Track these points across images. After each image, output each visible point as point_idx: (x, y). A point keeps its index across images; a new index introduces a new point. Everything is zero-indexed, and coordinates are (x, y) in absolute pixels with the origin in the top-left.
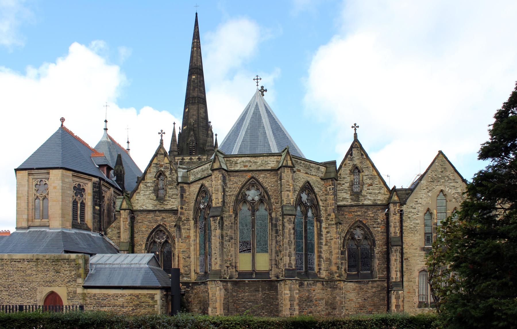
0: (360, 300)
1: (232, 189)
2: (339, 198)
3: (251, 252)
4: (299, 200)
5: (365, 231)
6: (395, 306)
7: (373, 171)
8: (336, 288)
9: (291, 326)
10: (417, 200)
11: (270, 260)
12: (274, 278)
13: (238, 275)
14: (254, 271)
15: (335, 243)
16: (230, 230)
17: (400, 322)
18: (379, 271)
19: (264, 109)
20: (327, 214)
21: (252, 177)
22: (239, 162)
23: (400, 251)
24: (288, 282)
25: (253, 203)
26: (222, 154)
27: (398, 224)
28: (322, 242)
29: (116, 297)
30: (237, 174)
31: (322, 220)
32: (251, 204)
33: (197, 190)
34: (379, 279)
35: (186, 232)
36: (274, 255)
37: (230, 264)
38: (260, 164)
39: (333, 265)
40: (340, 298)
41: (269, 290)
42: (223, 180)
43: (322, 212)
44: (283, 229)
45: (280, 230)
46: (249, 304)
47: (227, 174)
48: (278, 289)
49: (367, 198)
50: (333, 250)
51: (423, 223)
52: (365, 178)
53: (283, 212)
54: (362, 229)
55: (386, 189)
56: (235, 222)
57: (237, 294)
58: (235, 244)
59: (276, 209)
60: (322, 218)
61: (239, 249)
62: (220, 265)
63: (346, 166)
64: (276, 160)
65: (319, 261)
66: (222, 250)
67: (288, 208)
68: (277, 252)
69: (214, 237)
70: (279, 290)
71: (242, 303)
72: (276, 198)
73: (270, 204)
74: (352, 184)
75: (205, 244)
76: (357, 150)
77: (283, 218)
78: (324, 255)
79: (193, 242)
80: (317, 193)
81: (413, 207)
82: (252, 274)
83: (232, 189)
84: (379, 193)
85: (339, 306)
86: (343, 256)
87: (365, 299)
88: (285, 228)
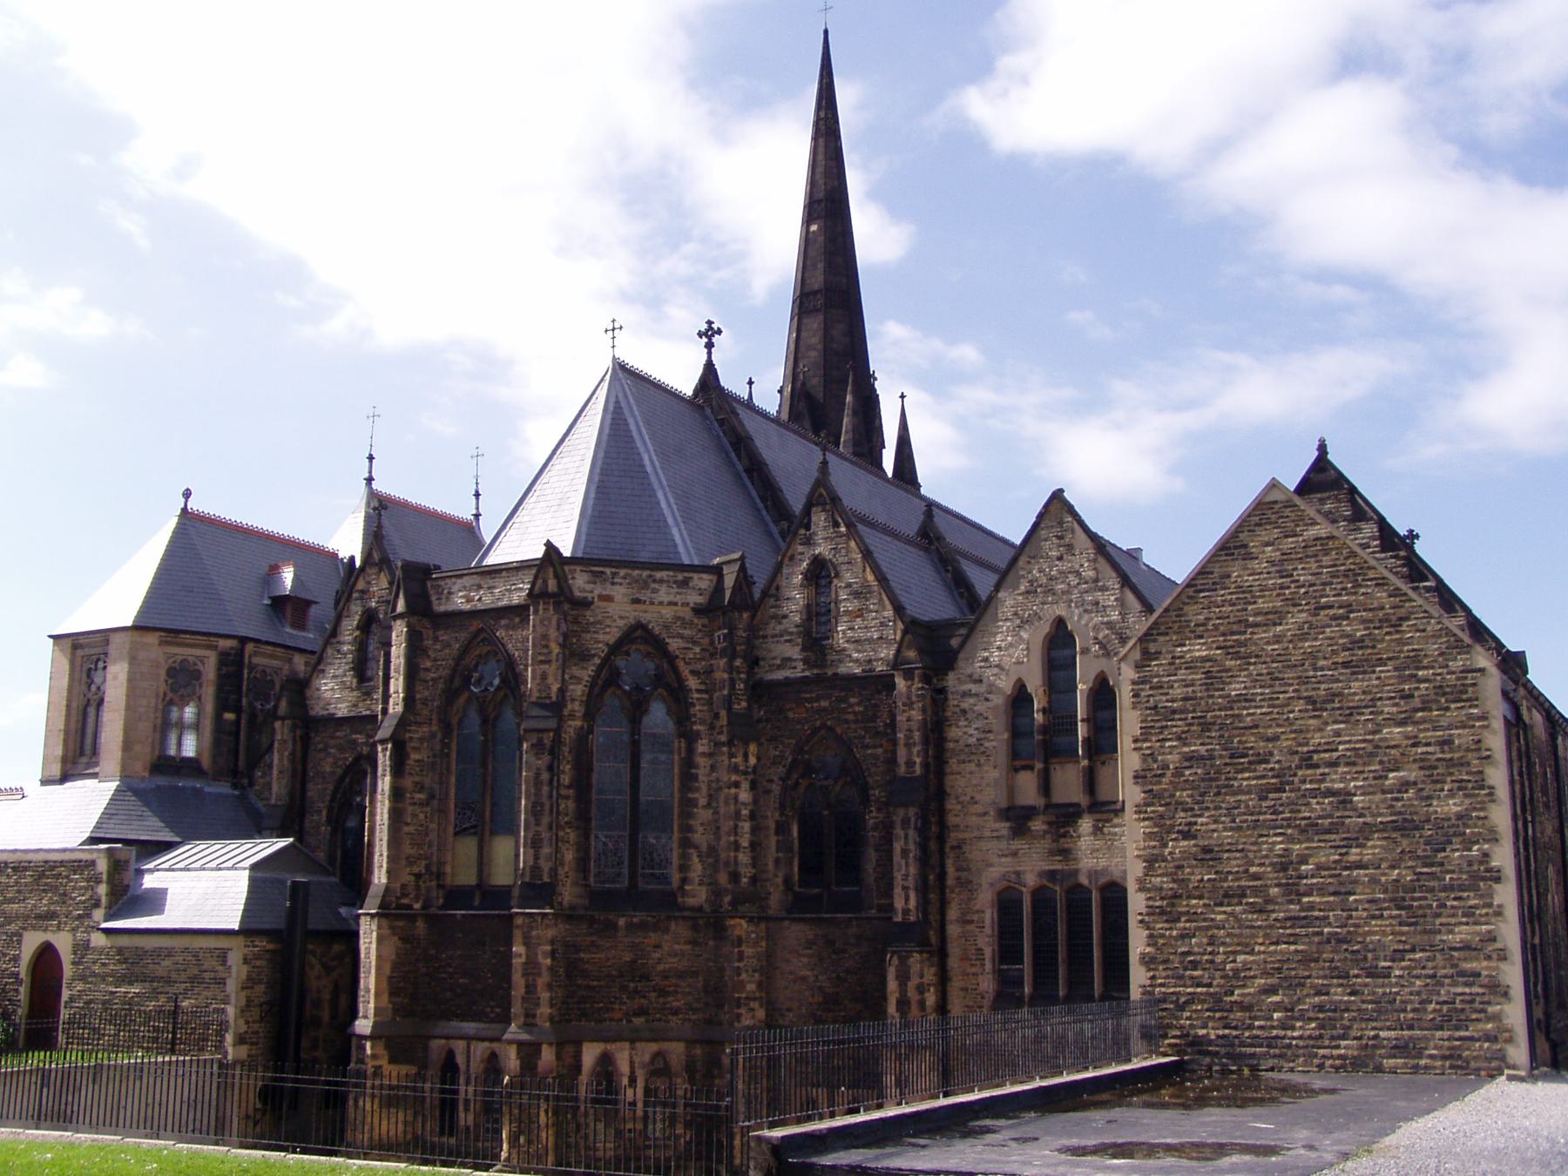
14: (479, 886)
28: (697, 799)
37: (427, 867)
43: (698, 708)
65: (684, 856)
78: (700, 837)
80: (677, 653)
81: (976, 676)
87: (838, 977)
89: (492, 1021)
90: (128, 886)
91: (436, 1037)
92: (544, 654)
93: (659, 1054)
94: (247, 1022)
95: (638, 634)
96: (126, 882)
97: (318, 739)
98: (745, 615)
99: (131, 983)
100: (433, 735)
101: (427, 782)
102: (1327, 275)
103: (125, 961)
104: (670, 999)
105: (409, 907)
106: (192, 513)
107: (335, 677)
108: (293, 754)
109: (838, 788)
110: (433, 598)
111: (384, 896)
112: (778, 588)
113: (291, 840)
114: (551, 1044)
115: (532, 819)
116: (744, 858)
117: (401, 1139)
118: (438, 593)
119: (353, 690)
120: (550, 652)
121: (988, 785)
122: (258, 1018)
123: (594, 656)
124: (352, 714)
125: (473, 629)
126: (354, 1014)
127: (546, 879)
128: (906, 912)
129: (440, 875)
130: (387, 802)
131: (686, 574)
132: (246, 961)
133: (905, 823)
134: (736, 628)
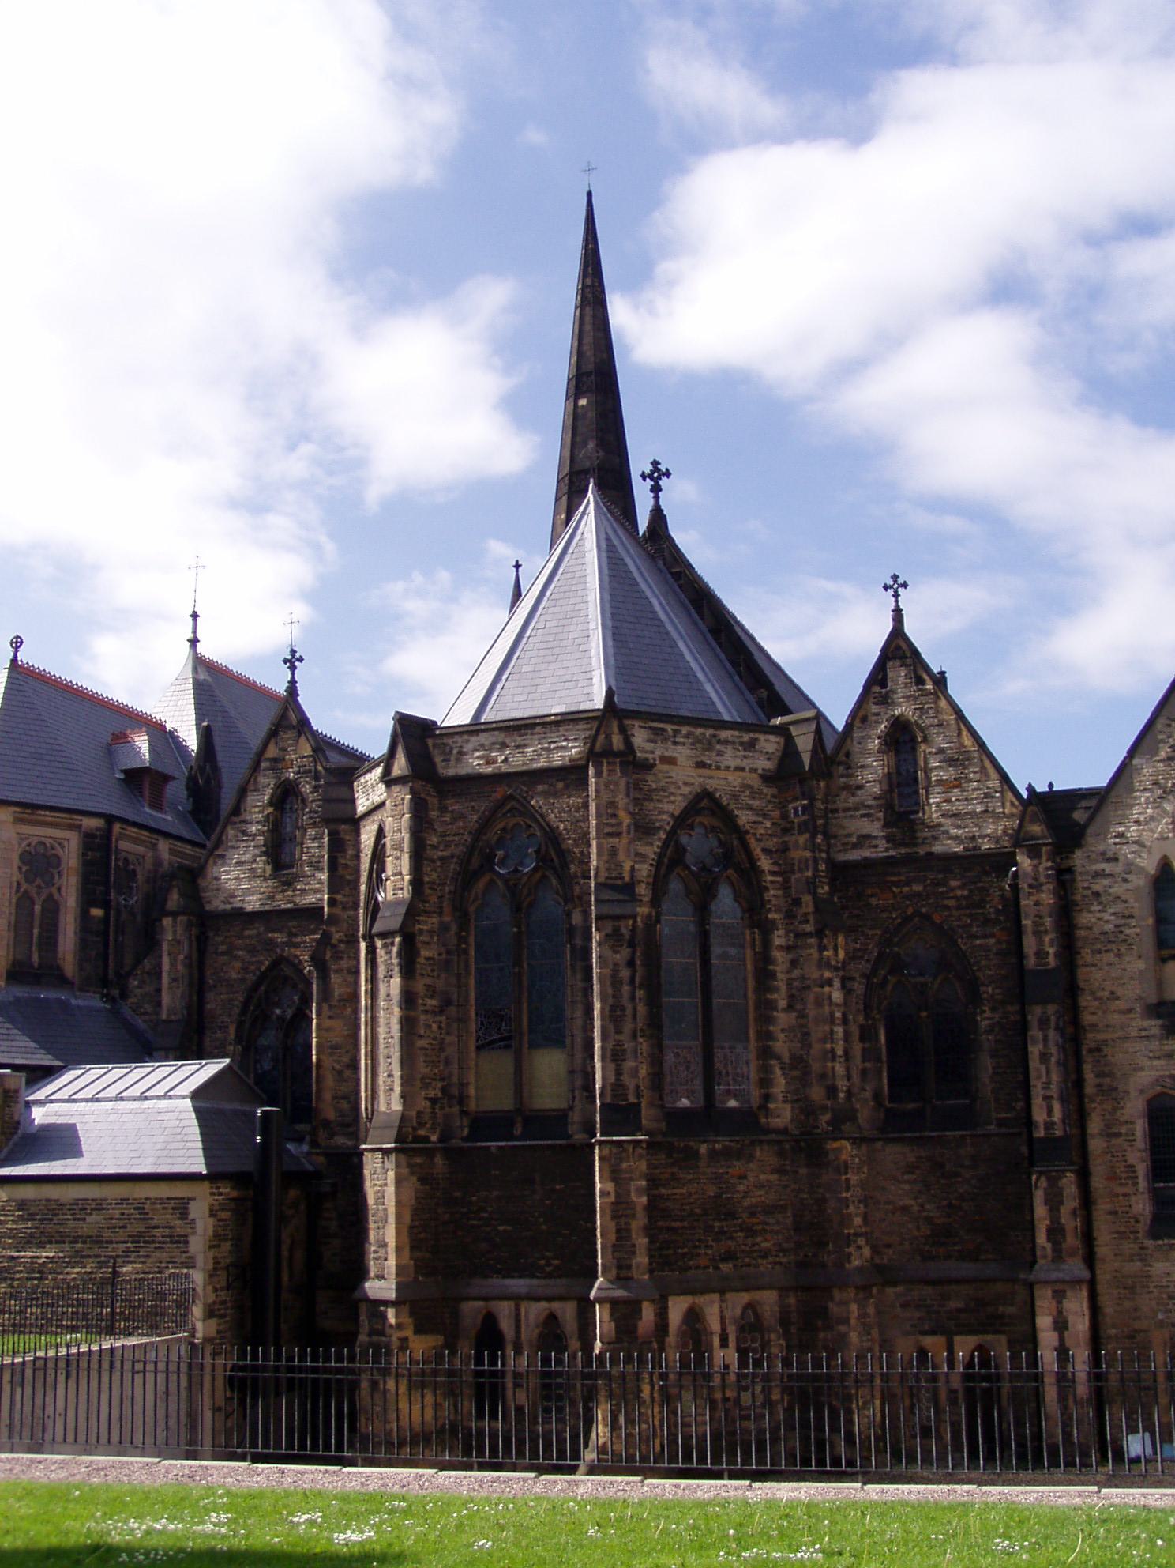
1: (451, 839)
13: (471, 1127)
28: (776, 1001)
29: (81, 1209)
37: (444, 1090)
46: (501, 1228)
65: (765, 1069)
80: (748, 827)
81: (1110, 854)
87: (950, 1206)
89: (549, 1276)
90: (18, 1123)
91: (468, 1299)
92: (613, 825)
93: (750, 1306)
94: (215, 1290)
95: (705, 804)
96: (16, 1118)
97: (219, 939)
98: (822, 784)
99: (41, 1245)
100: (444, 928)
101: (440, 985)
102: (942, 504)
103: (31, 1217)
104: (759, 1239)
105: (426, 1139)
106: (22, 667)
107: (240, 863)
108: (188, 957)
109: (936, 986)
110: (438, 760)
111: (400, 1127)
112: (848, 755)
113: (228, 1061)
114: (653, 1301)
115: (611, 1027)
116: (840, 1069)
117: (417, 1427)
118: (444, 753)
119: (266, 879)
120: (620, 824)
121: (1131, 978)
122: (224, 1284)
123: (659, 828)
124: (267, 908)
125: (498, 796)
126: (360, 1272)
127: (632, 1099)
128: (1049, 1126)
129: (462, 1099)
130: (397, 1010)
131: (752, 735)
132: (212, 1214)
133: (1044, 1023)
134: (815, 799)
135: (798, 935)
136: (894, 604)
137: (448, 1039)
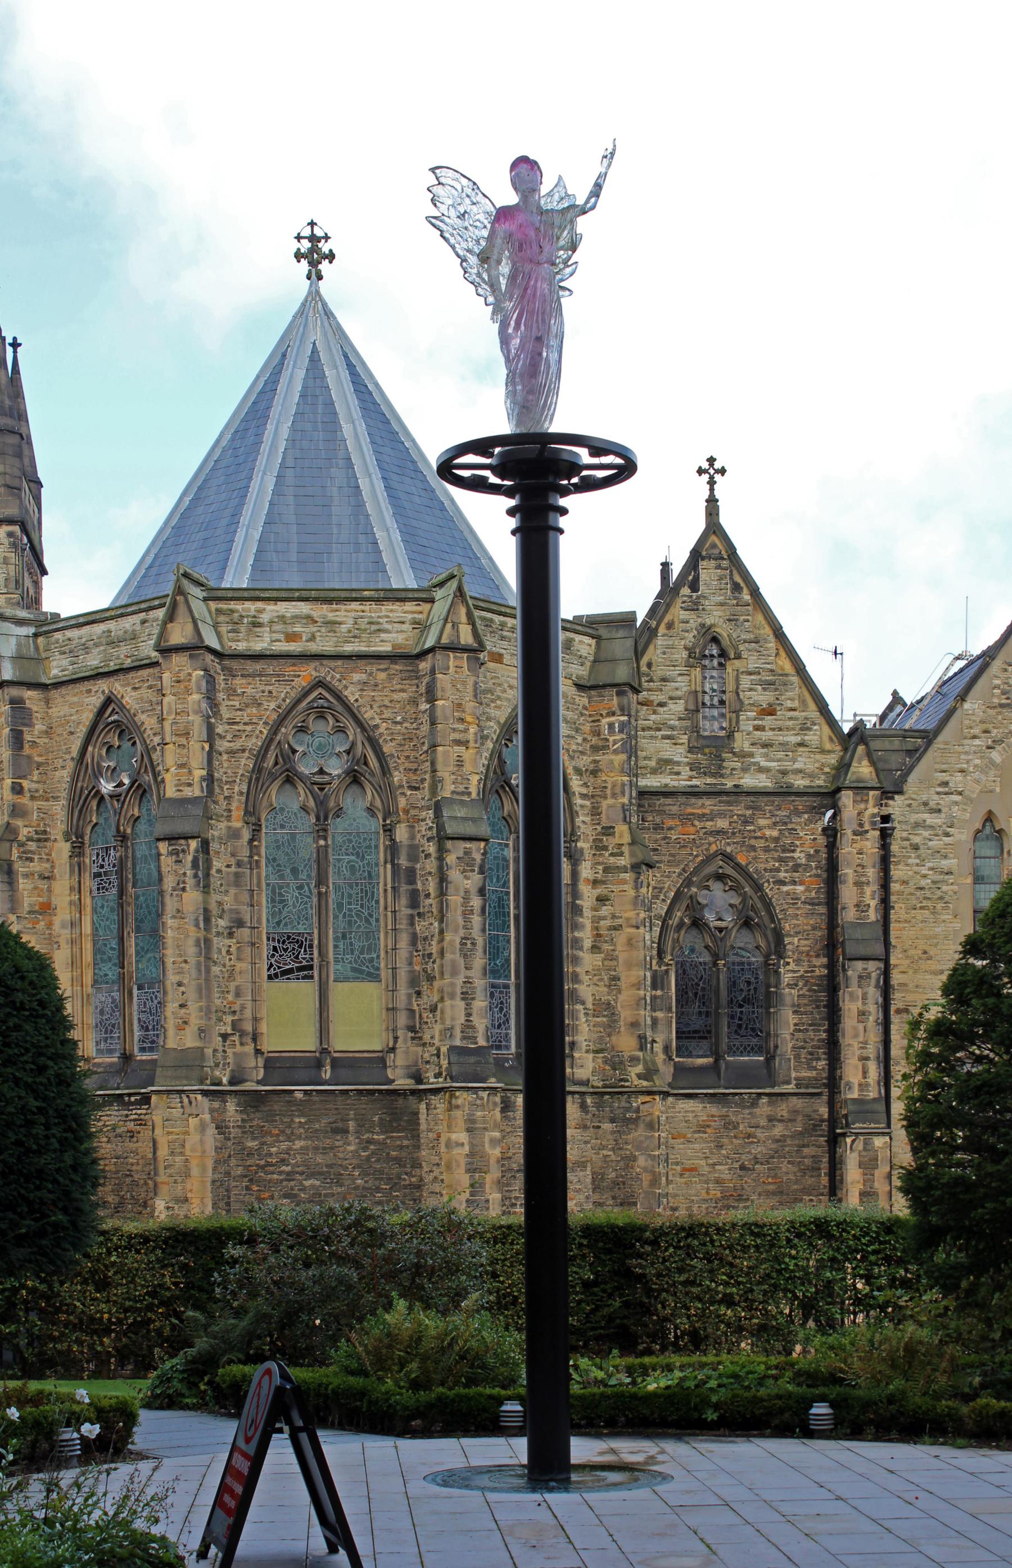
0: (723, 1171)
1: (241, 727)
2: (645, 758)
3: (312, 977)
4: (495, 772)
5: (744, 897)
6: (861, 1194)
7: (777, 655)
8: (635, 1121)
9: (581, 1237)
10: (947, 778)
11: (388, 1009)
12: (403, 1082)
13: (265, 1067)
15: (630, 942)
16: (233, 891)
17: (861, 1229)
18: (797, 1057)
19: (345, 375)
20: (599, 828)
21: (320, 684)
22: (265, 618)
23: (878, 980)
24: (463, 1098)
25: (322, 787)
26: (199, 584)
27: (872, 873)
28: (581, 940)
30: (258, 666)
31: (582, 850)
32: (316, 787)
33: (87, 717)
34: (798, 1086)
35: (36, 888)
36: (403, 990)
37: (234, 1025)
38: (349, 631)
39: (622, 1029)
40: (650, 1162)
41: (387, 1127)
42: (208, 690)
43: (581, 818)
44: (442, 893)
45: (428, 896)
47: (218, 667)
48: (419, 1124)
49: (754, 764)
50: (621, 971)
51: (968, 868)
52: (746, 681)
53: (441, 827)
54: (731, 888)
55: (826, 730)
56: (251, 857)
57: (263, 1144)
58: (253, 944)
59: (412, 812)
60: (579, 844)
61: (266, 967)
62: (201, 1030)
63: (672, 632)
64: (410, 616)
66: (208, 971)
67: (461, 812)
68: (414, 981)
69: (174, 917)
70: (423, 1126)
71: (282, 1181)
72: (414, 766)
73: (387, 791)
74: (696, 707)
75: (121, 940)
76: (719, 567)
77: (442, 851)
79: (68, 931)
81: (932, 804)
82: (319, 1065)
83: (241, 727)
84: (801, 744)
85: (646, 1193)
86: (659, 993)
88: (451, 890)
135: (607, 870)
136: (708, 493)
137: (239, 966)
